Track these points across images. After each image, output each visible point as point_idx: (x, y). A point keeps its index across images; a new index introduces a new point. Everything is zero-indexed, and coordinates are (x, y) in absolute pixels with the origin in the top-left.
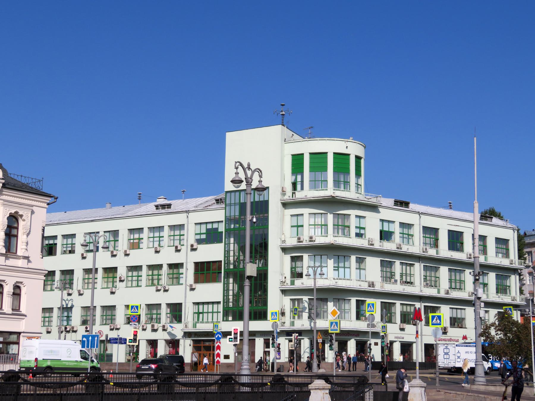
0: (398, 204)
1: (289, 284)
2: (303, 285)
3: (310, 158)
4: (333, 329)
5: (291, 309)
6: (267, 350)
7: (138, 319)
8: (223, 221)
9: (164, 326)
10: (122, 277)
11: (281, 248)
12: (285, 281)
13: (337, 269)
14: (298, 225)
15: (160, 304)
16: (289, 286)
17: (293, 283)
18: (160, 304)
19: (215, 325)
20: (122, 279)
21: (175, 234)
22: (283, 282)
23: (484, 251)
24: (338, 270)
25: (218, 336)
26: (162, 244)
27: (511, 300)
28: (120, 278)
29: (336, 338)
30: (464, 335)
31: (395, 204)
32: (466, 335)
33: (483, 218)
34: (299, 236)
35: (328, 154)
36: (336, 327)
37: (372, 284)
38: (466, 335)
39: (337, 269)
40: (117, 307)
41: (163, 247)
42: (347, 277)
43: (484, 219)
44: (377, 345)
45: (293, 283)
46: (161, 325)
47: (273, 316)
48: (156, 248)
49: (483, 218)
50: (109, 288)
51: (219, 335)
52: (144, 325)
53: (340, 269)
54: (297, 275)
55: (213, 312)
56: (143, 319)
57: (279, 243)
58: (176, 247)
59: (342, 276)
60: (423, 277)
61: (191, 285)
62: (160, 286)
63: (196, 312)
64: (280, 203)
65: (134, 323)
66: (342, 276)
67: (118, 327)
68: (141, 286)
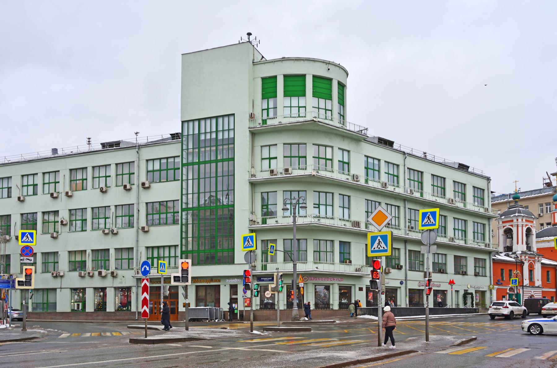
0: (382, 143)
1: (260, 223)
2: (278, 223)
3: (285, 81)
4: (376, 249)
5: (262, 251)
6: (234, 297)
7: (83, 265)
8: (179, 156)
9: (112, 273)
10: (63, 220)
11: (249, 182)
12: (117, 232)
13: (317, 206)
14: (270, 157)
15: (108, 250)
16: (260, 226)
17: (264, 222)
18: (108, 250)
19: (161, 264)
20: (64, 223)
21: (124, 173)
22: (252, 221)
23: (464, 198)
24: (319, 207)
25: (145, 268)
26: (108, 185)
27: (257, 298)
28: (62, 222)
29: (177, 269)
30: (450, 280)
31: (378, 141)
32: (453, 280)
33: (460, 167)
34: (272, 168)
35: (307, 77)
36: (383, 245)
37: (357, 224)
38: (453, 280)
39: (317, 206)
40: (59, 253)
41: (110, 187)
42: (329, 214)
43: (462, 167)
44: (359, 288)
45: (264, 222)
46: (110, 272)
47: (246, 243)
48: (102, 188)
49: (460, 167)
50: (50, 233)
51: (146, 266)
52: (90, 272)
53: (321, 206)
54: (268, 213)
55: (479, 267)
56: (89, 265)
57: (247, 177)
58: (125, 187)
59: (323, 214)
60: (407, 221)
61: (143, 228)
62: (107, 230)
63: (150, 257)
64: (248, 132)
65: (28, 258)
66: (323, 214)
67: (62, 274)
68: (86, 231)
